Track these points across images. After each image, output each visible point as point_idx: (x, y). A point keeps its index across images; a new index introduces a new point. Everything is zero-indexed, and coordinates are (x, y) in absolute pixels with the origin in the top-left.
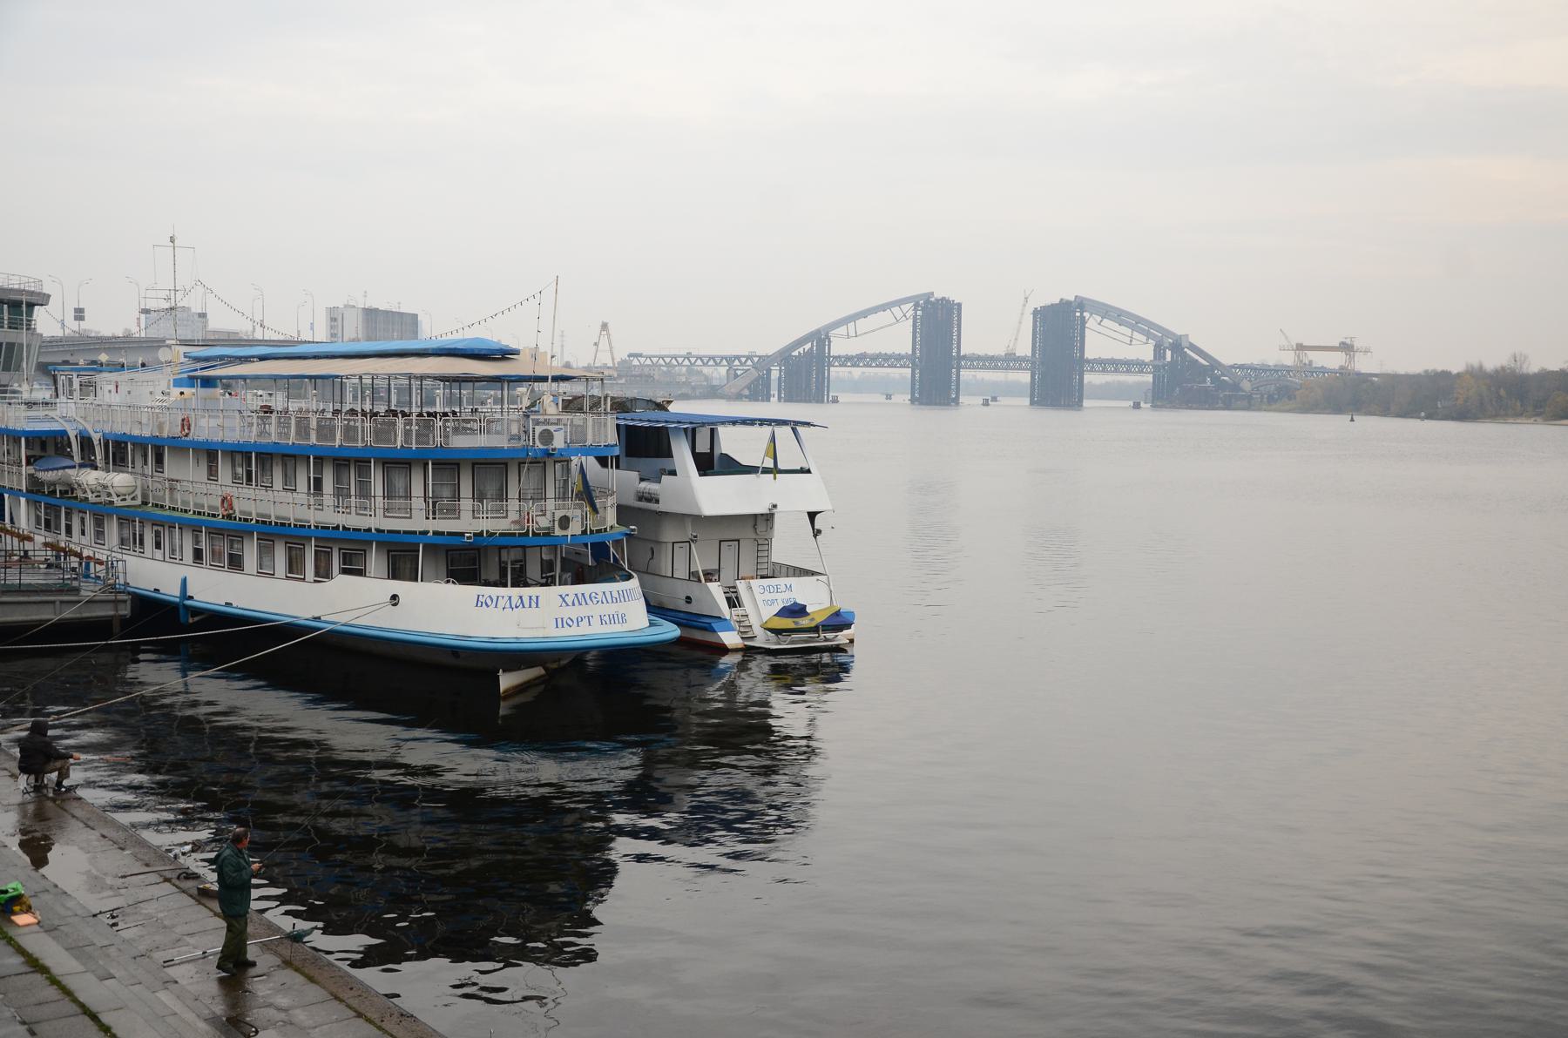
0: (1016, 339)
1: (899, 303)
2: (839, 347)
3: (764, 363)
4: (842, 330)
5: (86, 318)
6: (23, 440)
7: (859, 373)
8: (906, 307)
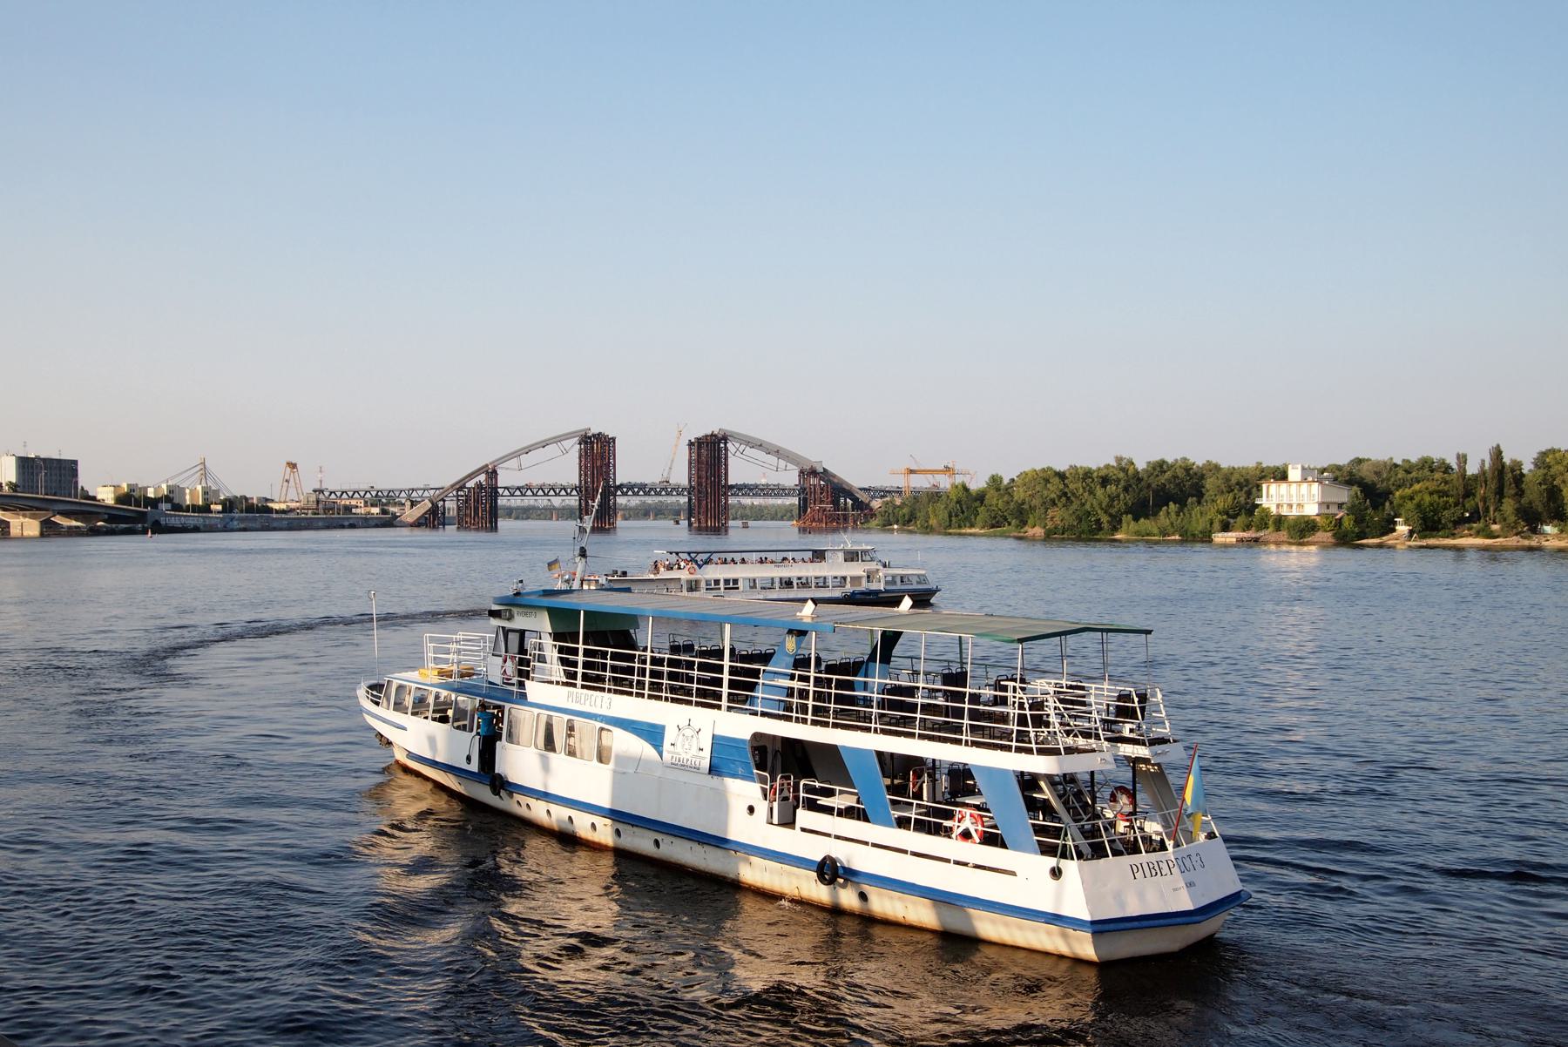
0: (670, 468)
1: (558, 439)
2: (503, 480)
3: (443, 493)
4: (513, 463)
5: (1464, 452)
6: (651, 618)
7: (560, 501)
8: (567, 444)
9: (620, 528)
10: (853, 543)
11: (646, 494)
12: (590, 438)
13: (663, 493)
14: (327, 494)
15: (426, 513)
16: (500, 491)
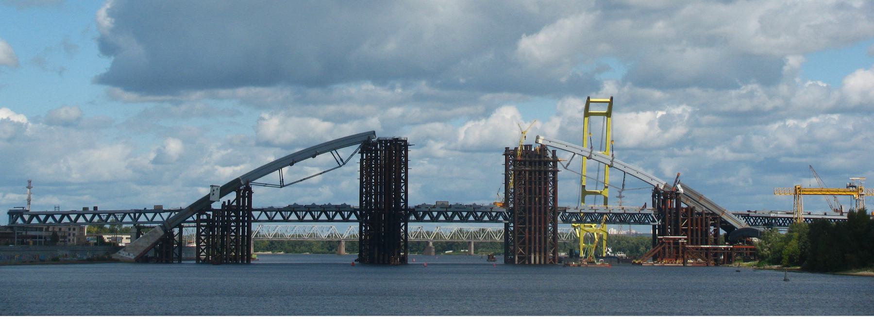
2: (261, 196)
3: (181, 217)
8: (344, 153)
9: (630, 226)
10: (591, 227)
11: (464, 220)
12: (375, 144)
13: (457, 218)
14: (26, 217)
15: (156, 243)
16: (255, 214)
